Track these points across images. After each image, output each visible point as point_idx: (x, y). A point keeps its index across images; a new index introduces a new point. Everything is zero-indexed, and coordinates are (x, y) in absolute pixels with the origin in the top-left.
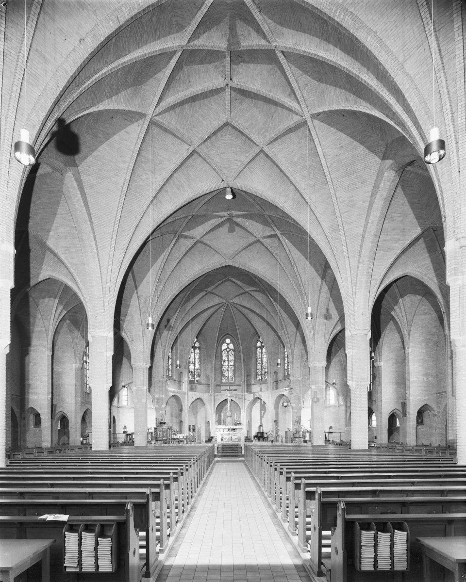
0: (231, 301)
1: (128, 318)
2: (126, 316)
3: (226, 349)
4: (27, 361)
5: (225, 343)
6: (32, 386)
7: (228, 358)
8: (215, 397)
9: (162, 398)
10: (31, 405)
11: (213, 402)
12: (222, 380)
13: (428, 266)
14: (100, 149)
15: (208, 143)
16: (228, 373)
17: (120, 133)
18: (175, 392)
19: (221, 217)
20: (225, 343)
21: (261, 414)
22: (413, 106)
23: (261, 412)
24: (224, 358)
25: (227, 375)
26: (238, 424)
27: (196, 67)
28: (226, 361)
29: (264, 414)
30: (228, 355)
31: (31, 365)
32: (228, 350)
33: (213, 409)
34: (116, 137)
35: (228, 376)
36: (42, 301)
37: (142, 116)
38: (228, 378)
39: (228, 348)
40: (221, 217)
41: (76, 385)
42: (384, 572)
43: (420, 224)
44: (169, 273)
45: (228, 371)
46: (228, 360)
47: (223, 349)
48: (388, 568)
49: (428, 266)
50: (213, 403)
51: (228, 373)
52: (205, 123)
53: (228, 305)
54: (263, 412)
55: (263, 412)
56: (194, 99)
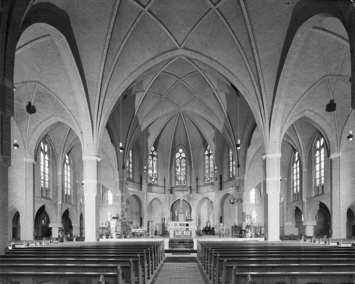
3: (179, 158)
12: (175, 183)
16: (181, 177)
20: (183, 152)
24: (177, 165)
25: (180, 179)
28: (179, 168)
33: (168, 206)
35: (181, 180)
38: (181, 182)
39: (181, 156)
45: (181, 175)
46: (181, 167)
51: (181, 177)
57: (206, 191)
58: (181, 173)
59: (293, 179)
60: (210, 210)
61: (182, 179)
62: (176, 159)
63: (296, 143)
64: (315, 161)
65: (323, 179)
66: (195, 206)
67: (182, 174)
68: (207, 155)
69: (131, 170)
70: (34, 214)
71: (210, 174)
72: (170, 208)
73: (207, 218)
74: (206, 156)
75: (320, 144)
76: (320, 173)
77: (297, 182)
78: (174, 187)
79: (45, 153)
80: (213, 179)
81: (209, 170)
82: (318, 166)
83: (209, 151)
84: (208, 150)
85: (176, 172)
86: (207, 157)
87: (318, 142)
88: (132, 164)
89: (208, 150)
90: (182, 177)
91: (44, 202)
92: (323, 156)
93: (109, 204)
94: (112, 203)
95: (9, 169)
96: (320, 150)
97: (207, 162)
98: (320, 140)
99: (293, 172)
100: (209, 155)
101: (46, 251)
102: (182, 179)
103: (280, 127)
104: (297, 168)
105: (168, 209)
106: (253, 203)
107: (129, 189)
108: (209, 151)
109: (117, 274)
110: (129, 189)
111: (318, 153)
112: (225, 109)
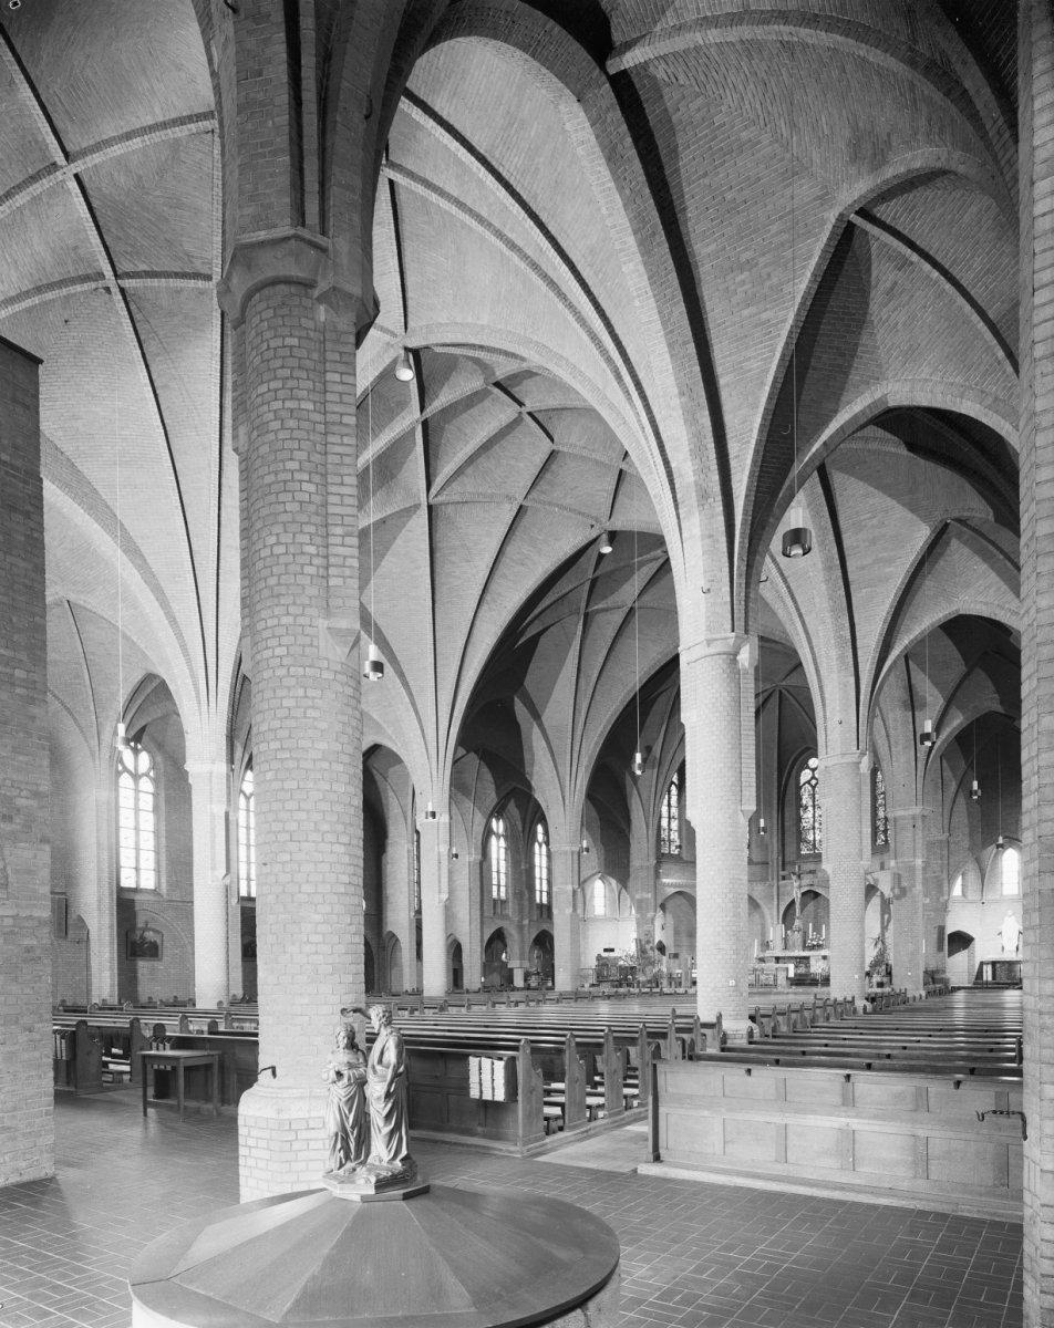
0: (784, 683)
1: (536, 768)
2: (532, 765)
3: (808, 782)
4: (384, 861)
5: (808, 767)
6: (391, 899)
7: (814, 802)
8: (781, 889)
9: (648, 899)
10: (389, 928)
11: (776, 900)
12: (799, 849)
13: (999, 589)
14: (383, 564)
15: (543, 485)
16: (814, 834)
17: (401, 535)
18: (680, 886)
19: (656, 559)
20: (808, 767)
21: (882, 923)
22: (727, 385)
23: (883, 918)
24: (804, 802)
25: (811, 839)
26: (814, 946)
27: (465, 416)
28: (810, 809)
29: (889, 921)
30: (814, 795)
31: (389, 866)
32: (813, 782)
33: (775, 913)
34: (399, 541)
35: (814, 840)
36: (391, 770)
37: (417, 507)
38: (814, 845)
39: (813, 777)
40: (656, 559)
41: (470, 890)
42: (486, 1101)
43: (924, 519)
44: (596, 675)
45: (814, 828)
46: (814, 806)
47: (802, 783)
48: (478, 1097)
49: (999, 589)
50: (776, 903)
51: (814, 834)
52: (521, 465)
53: (780, 691)
54: (886, 916)
55: (886, 916)
56: (486, 447)
58: (814, 821)
62: (801, 788)
69: (676, 834)
70: (482, 941)
72: (781, 913)
79: (498, 836)
85: (799, 819)
88: (677, 821)
91: (499, 923)
95: (519, 53)
101: (535, 1028)
105: (775, 918)
106: (1011, 893)
107: (664, 880)
109: (514, 989)
110: (664, 880)
112: (669, 801)
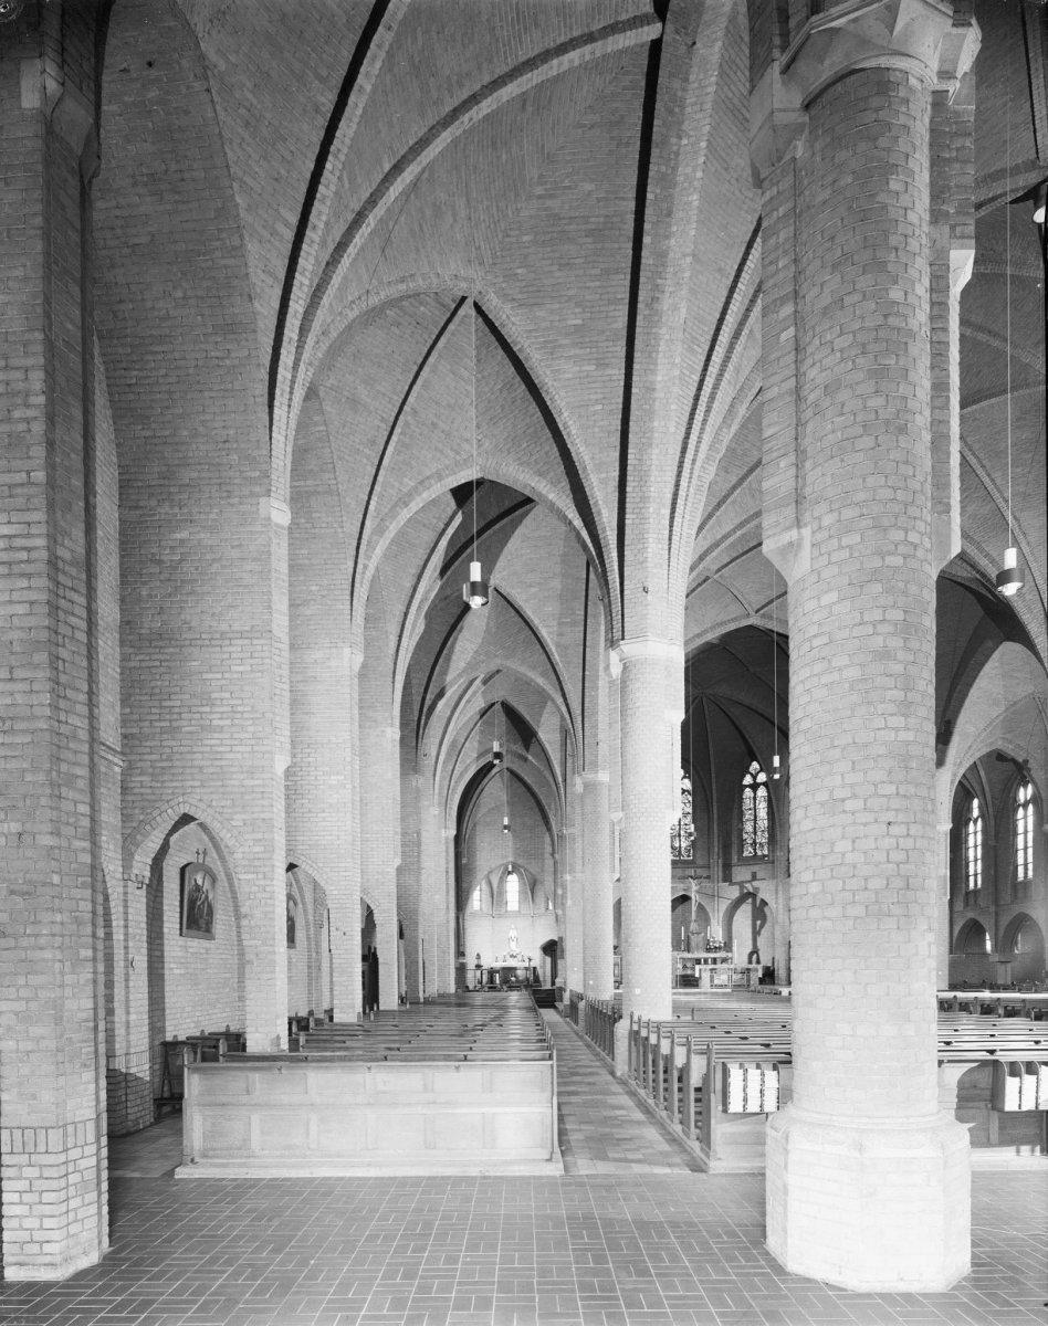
38: (680, 852)
45: (680, 835)
57: (749, 877)
59: (967, 858)
60: (759, 922)
61: (683, 845)
63: (975, 785)
64: (1015, 827)
65: (1030, 867)
66: (721, 915)
67: (682, 833)
68: (750, 786)
71: (759, 833)
73: (750, 942)
74: (748, 789)
75: (1026, 794)
76: (1026, 853)
77: (976, 871)
78: (549, 829)
80: (766, 848)
81: (755, 823)
82: (1020, 839)
83: (754, 777)
84: (751, 774)
86: (748, 792)
87: (1022, 789)
89: (751, 774)
90: (683, 839)
92: (1031, 820)
93: (509, 909)
94: (517, 908)
96: (1025, 806)
97: (748, 804)
98: (1025, 786)
99: (967, 841)
100: (754, 787)
102: (683, 845)
103: (950, 775)
104: (975, 833)
108: (754, 777)
111: (1021, 812)
